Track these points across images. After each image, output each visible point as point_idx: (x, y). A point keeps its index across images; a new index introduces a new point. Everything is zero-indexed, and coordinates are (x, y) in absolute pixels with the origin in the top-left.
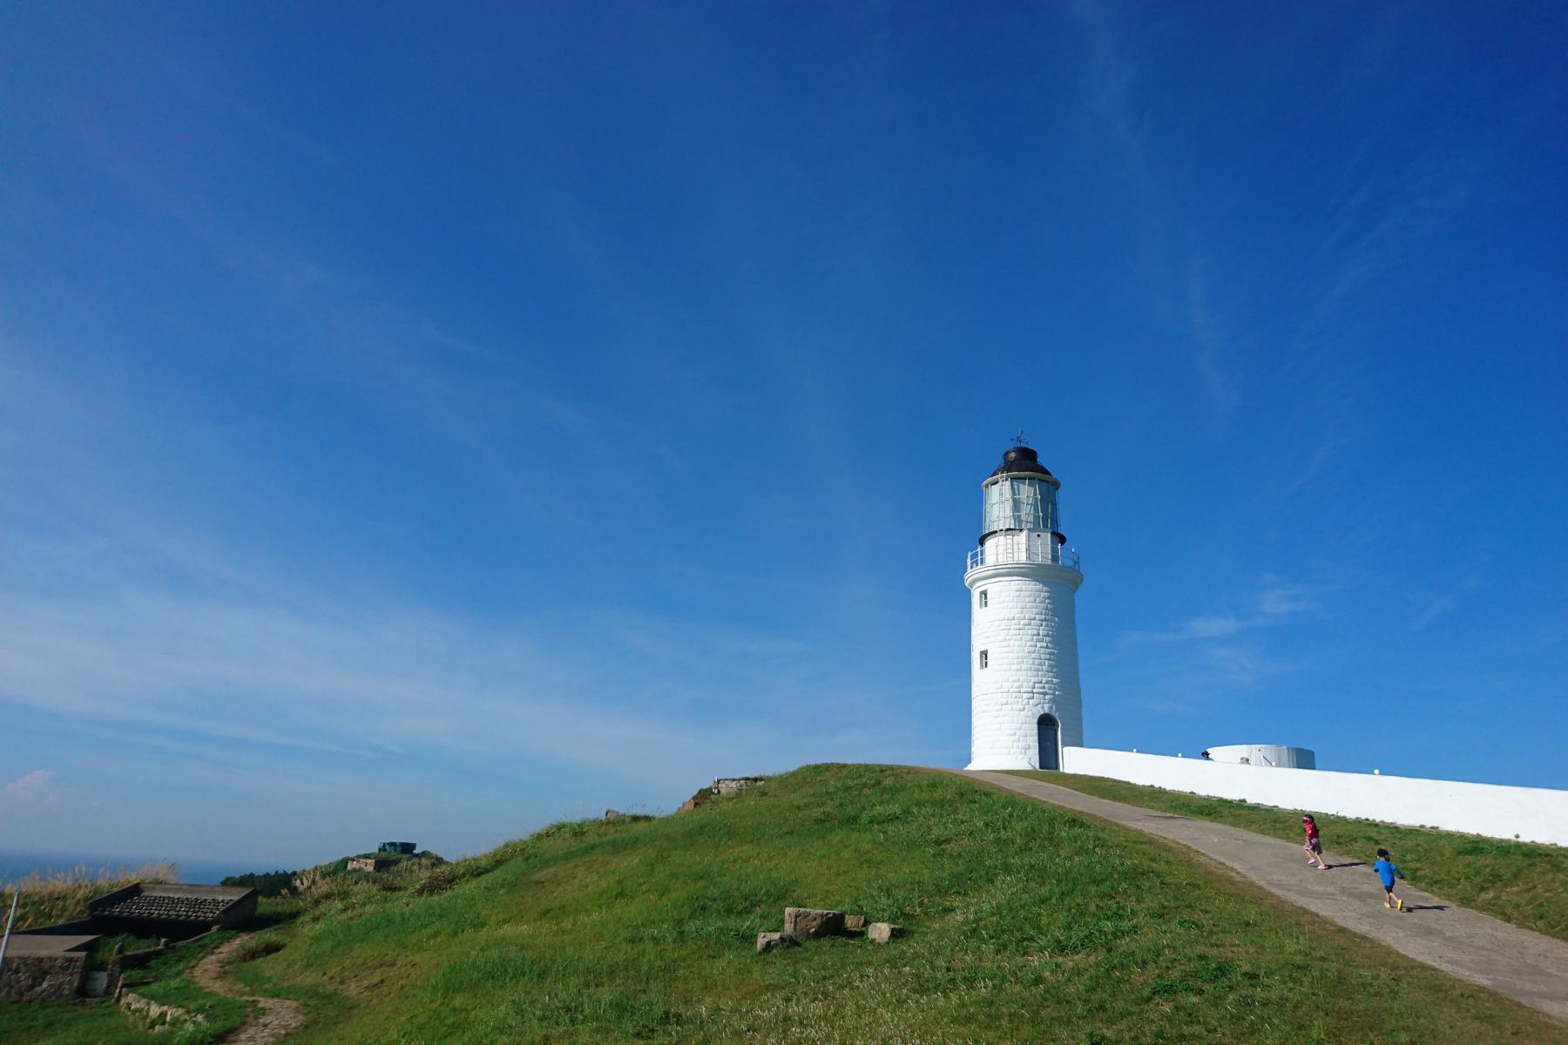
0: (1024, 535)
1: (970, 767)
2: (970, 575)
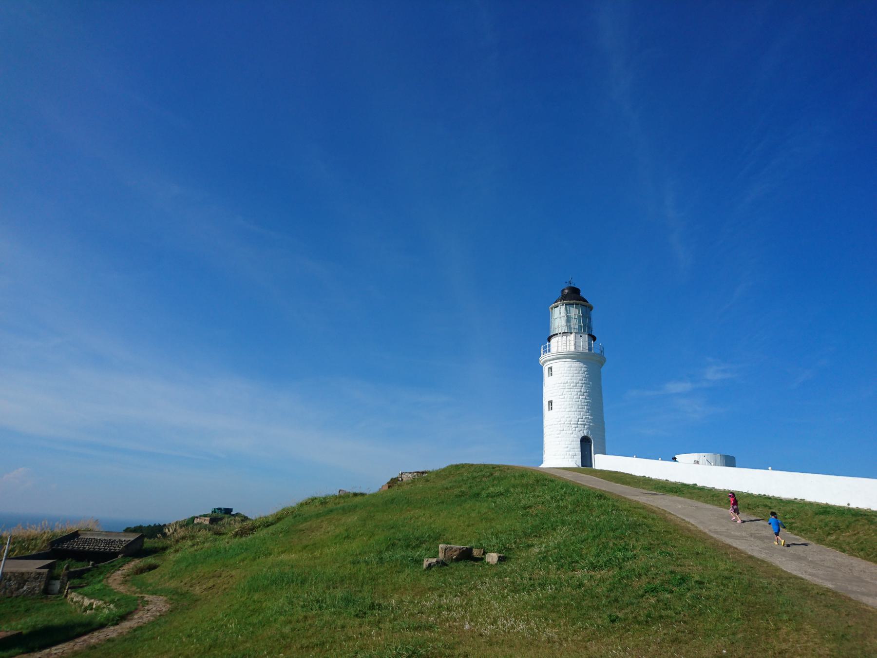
0: (573, 336)
1: (543, 466)
2: (543, 358)
